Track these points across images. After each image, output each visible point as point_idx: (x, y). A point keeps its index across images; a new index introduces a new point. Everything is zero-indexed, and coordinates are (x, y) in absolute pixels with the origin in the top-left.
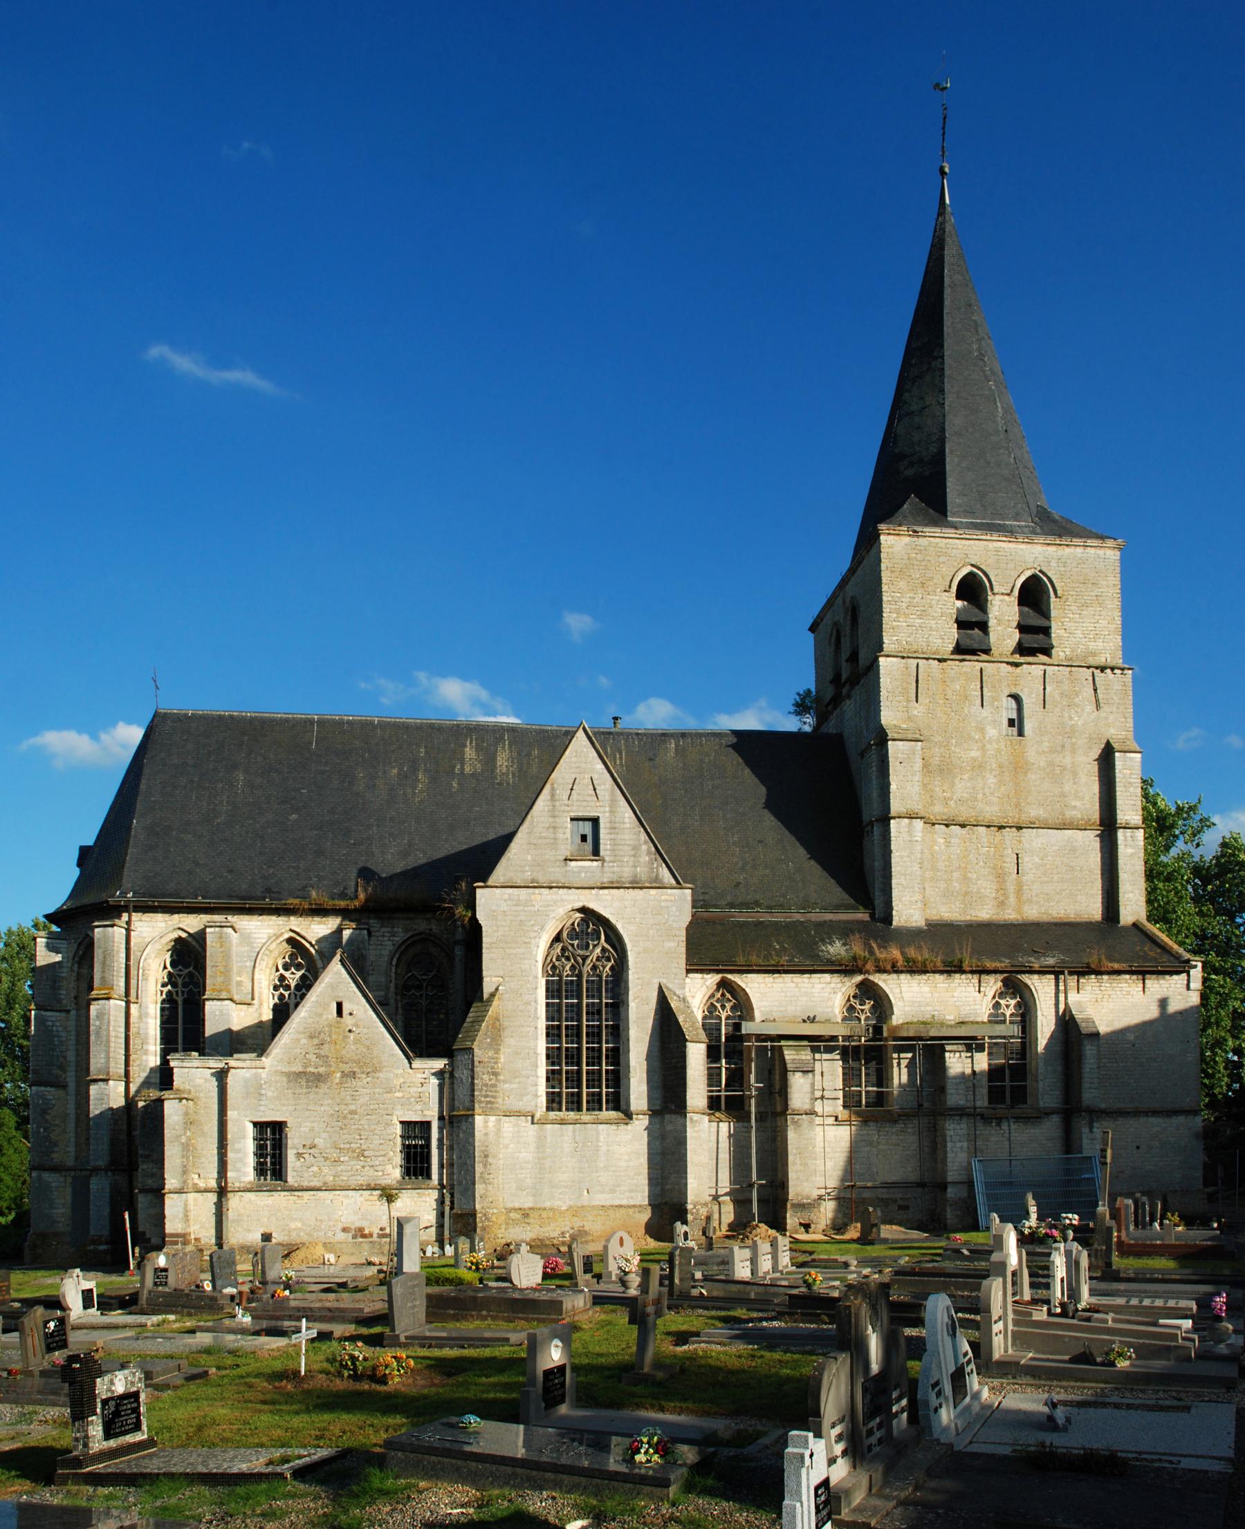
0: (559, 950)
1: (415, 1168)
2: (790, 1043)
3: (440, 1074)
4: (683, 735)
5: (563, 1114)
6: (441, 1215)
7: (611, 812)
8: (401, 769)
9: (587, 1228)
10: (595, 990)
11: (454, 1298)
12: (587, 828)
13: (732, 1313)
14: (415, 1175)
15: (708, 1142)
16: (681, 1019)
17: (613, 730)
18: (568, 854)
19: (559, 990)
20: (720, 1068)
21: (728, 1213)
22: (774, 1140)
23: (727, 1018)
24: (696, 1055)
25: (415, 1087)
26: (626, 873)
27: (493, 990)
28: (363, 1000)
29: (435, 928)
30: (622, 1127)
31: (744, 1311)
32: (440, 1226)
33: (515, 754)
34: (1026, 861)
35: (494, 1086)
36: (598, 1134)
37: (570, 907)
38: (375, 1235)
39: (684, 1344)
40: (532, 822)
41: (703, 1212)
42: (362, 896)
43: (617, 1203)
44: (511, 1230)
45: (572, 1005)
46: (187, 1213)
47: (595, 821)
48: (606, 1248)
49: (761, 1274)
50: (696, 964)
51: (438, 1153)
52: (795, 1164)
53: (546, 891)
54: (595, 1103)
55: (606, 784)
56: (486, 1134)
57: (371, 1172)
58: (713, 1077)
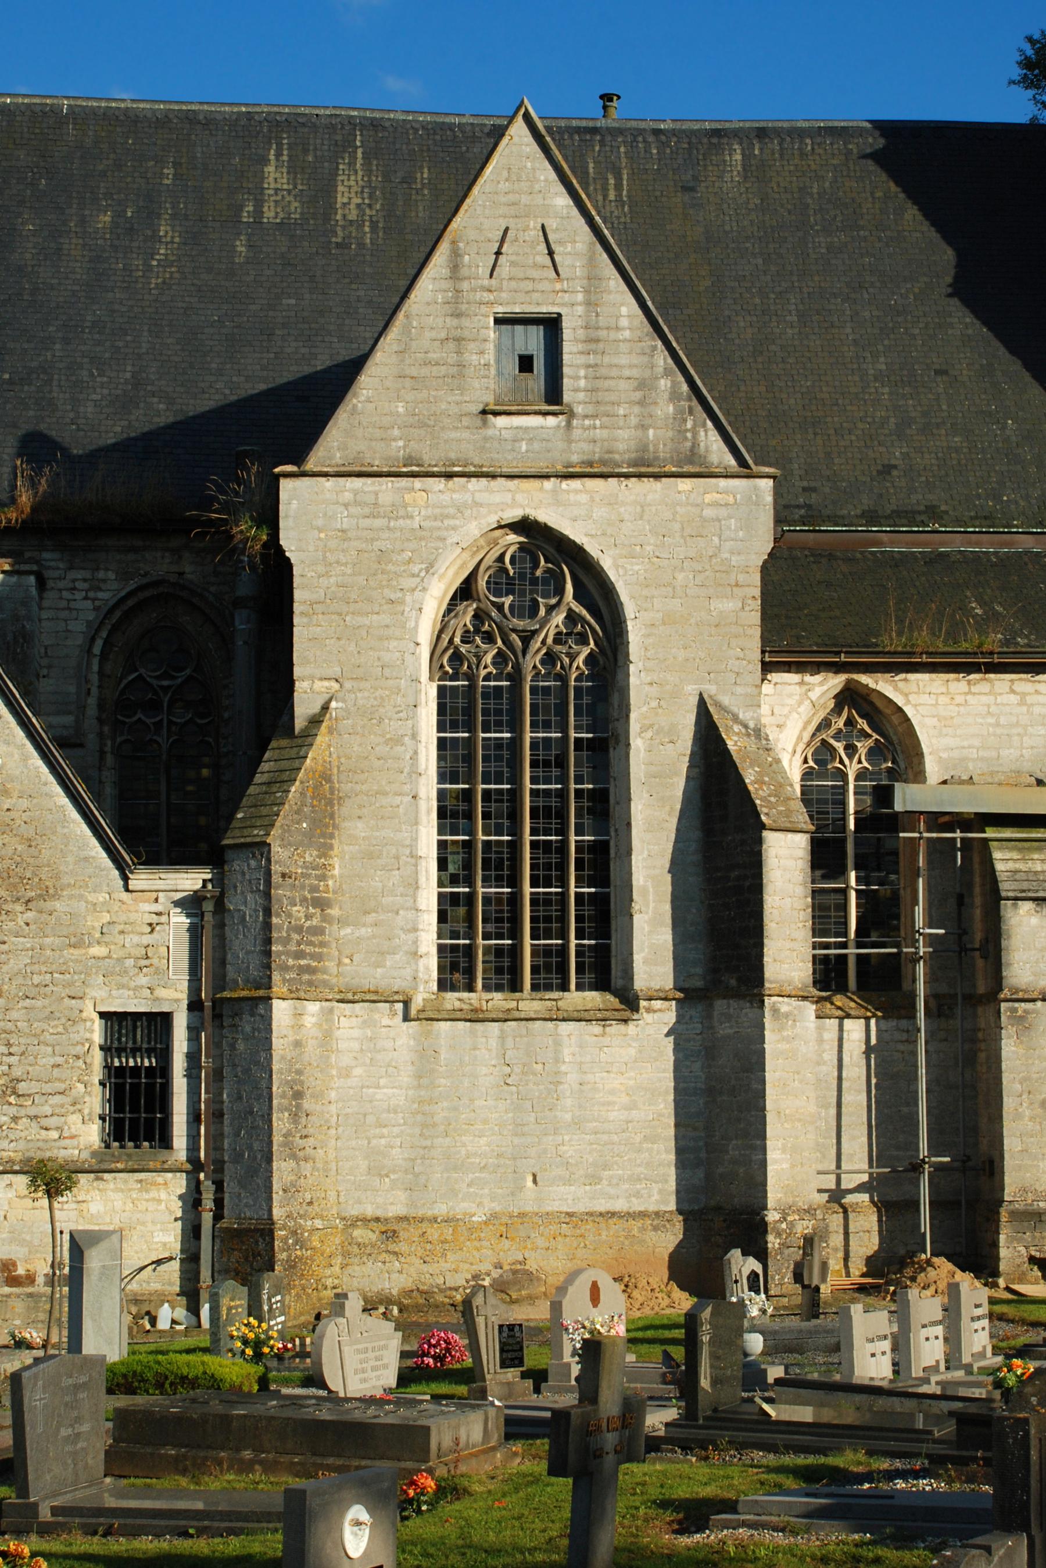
0: (468, 619)
1: (134, 1122)
2: (1008, 833)
3: (192, 904)
4: (762, 133)
6: (192, 1232)
7: (588, 303)
8: (119, 214)
9: (532, 1266)
10: (551, 711)
11: (178, 1419)
12: (533, 341)
13: (832, 1460)
14: (135, 1138)
15: (814, 1067)
16: (749, 777)
17: (601, 123)
18: (489, 398)
19: (469, 711)
20: (844, 892)
21: (867, 1234)
22: (970, 1060)
23: (859, 777)
24: (786, 860)
25: (131, 933)
26: (623, 441)
27: (316, 708)
28: (20, 733)
29: (190, 570)
30: (615, 1028)
31: (861, 1456)
32: (191, 1259)
33: (377, 179)
35: (318, 931)
36: (558, 1044)
37: (492, 521)
38: (40, 1280)
39: (700, 1530)
40: (407, 329)
41: (804, 1227)
42: (25, 499)
43: (602, 1206)
44: (356, 1270)
45: (499, 744)
47: (552, 325)
48: (556, 1308)
49: (916, 1372)
50: (785, 648)
51: (188, 1087)
52: (1018, 1116)
53: (439, 484)
54: (552, 974)
55: (575, 240)
56: (298, 1044)
57: (33, 1131)
58: (825, 914)
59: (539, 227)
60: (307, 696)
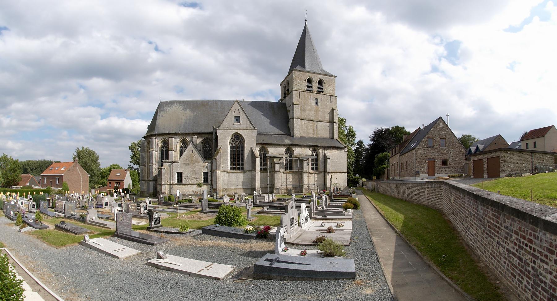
5: (233, 171)
25: (203, 166)
34: (318, 127)
46: (165, 188)
51: (208, 178)
59: (329, 110)
60: (219, 146)
